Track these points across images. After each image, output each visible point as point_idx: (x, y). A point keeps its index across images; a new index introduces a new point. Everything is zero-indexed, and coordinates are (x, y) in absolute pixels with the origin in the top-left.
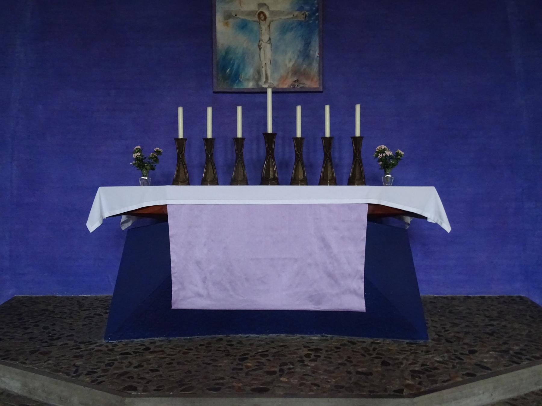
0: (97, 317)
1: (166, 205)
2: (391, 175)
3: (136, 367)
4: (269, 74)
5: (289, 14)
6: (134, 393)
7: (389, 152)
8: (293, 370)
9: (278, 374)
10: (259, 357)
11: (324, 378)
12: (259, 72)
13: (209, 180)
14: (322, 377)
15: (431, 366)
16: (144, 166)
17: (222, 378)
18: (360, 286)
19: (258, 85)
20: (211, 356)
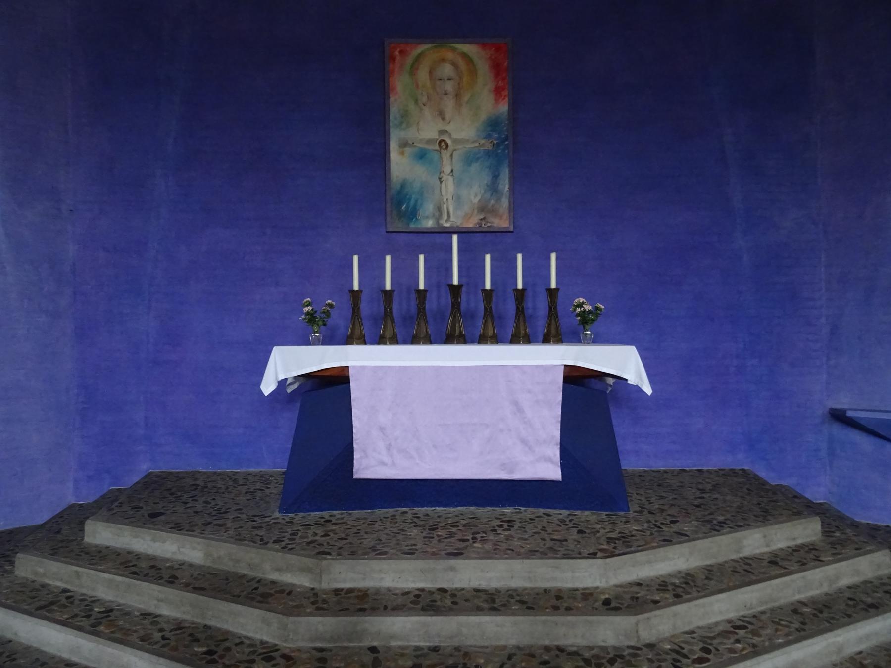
0: (260, 492)
1: (348, 367)
2: (590, 331)
3: (322, 536)
5: (474, 142)
6: (328, 557)
7: (588, 306)
8: (486, 538)
9: (471, 541)
10: (450, 527)
11: (517, 545)
12: (439, 209)
13: (388, 337)
14: (516, 543)
15: (628, 534)
16: (316, 321)
17: (415, 545)
18: (555, 452)
19: (438, 223)
20: (398, 527)
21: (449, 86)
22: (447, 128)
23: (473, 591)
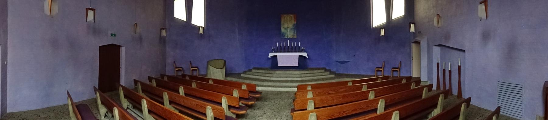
12: (288, 36)
21: (289, 20)
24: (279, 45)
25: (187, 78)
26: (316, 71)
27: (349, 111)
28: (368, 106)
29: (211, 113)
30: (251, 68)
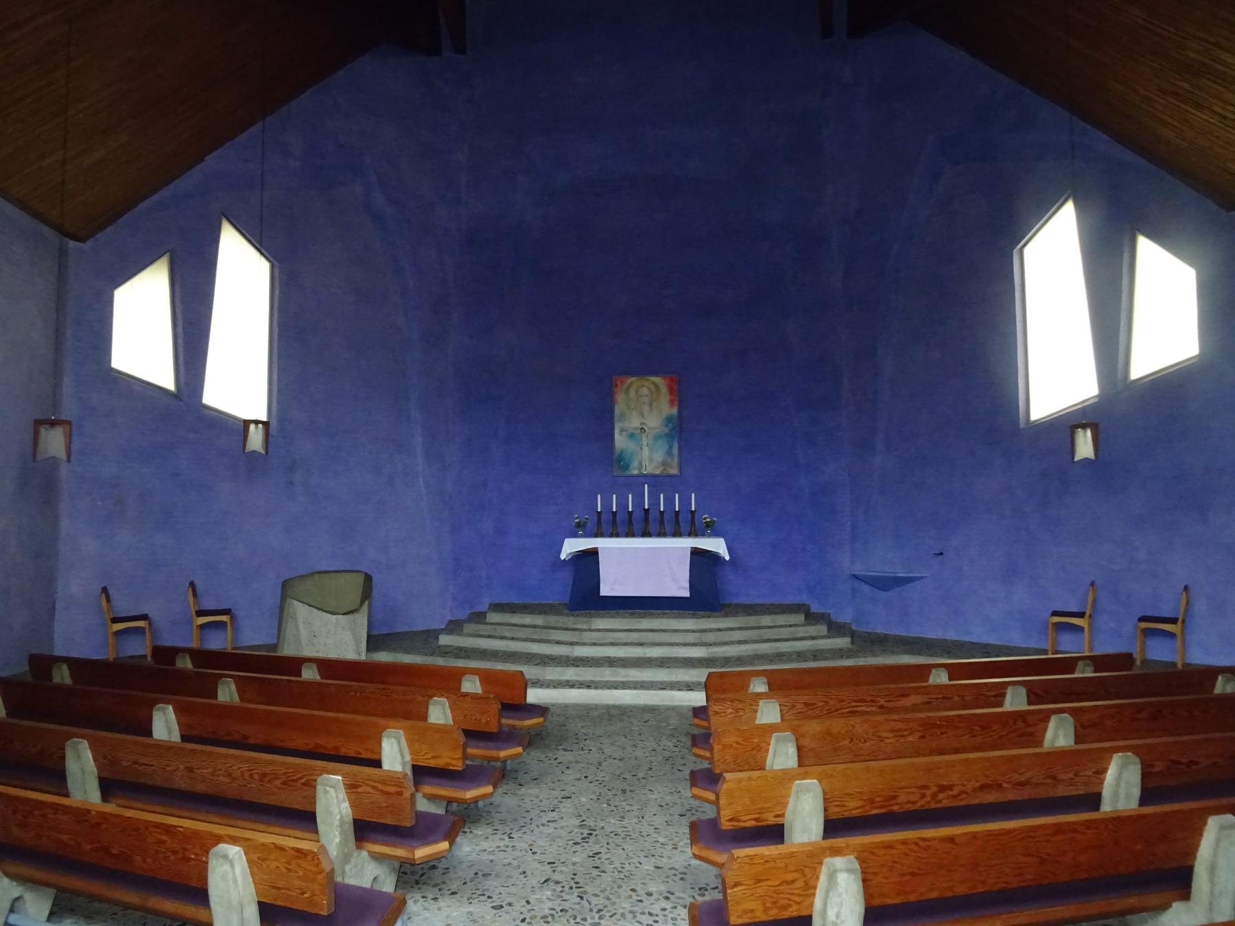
4: (647, 465)
12: (641, 464)
21: (646, 399)
22: (645, 421)
23: (691, 714)
24: (607, 503)
25: (185, 663)
26: (766, 620)
27: (963, 785)
28: (1054, 778)
29: (339, 804)
30: (483, 607)
